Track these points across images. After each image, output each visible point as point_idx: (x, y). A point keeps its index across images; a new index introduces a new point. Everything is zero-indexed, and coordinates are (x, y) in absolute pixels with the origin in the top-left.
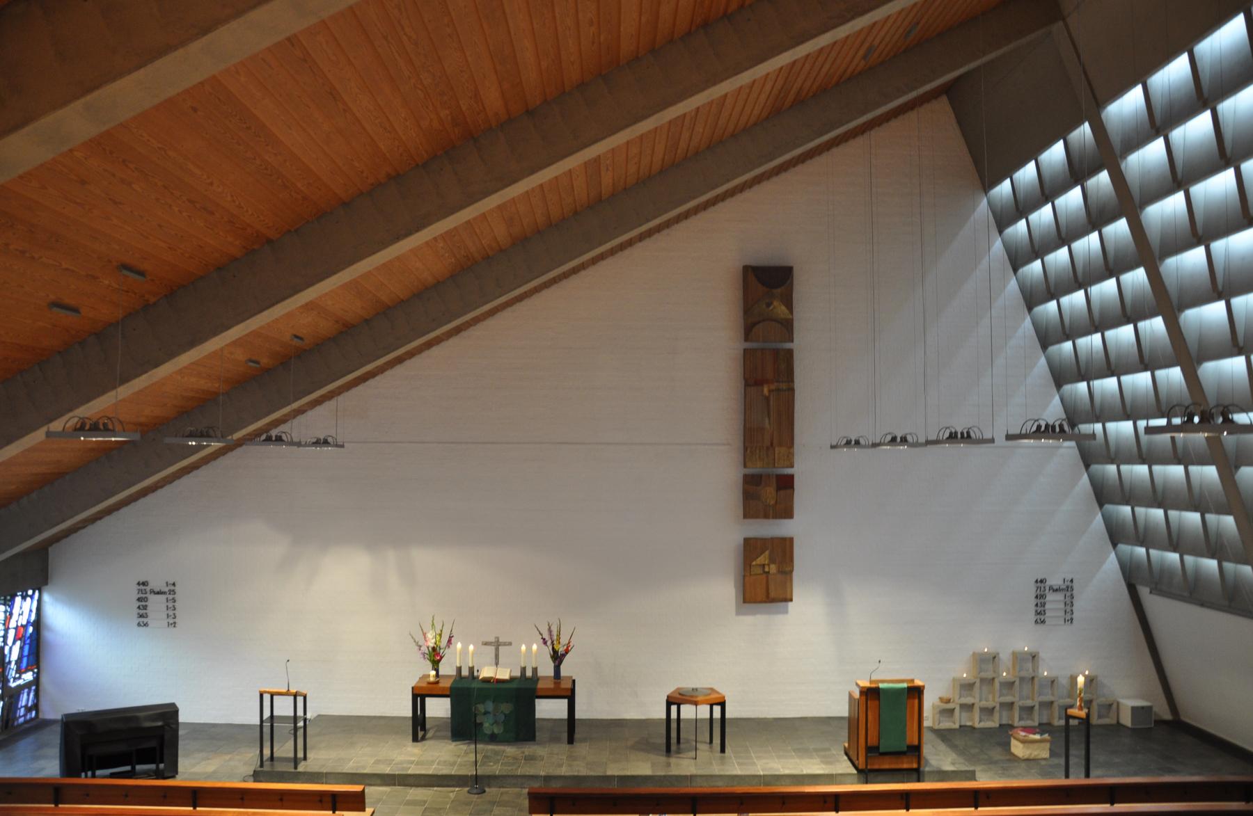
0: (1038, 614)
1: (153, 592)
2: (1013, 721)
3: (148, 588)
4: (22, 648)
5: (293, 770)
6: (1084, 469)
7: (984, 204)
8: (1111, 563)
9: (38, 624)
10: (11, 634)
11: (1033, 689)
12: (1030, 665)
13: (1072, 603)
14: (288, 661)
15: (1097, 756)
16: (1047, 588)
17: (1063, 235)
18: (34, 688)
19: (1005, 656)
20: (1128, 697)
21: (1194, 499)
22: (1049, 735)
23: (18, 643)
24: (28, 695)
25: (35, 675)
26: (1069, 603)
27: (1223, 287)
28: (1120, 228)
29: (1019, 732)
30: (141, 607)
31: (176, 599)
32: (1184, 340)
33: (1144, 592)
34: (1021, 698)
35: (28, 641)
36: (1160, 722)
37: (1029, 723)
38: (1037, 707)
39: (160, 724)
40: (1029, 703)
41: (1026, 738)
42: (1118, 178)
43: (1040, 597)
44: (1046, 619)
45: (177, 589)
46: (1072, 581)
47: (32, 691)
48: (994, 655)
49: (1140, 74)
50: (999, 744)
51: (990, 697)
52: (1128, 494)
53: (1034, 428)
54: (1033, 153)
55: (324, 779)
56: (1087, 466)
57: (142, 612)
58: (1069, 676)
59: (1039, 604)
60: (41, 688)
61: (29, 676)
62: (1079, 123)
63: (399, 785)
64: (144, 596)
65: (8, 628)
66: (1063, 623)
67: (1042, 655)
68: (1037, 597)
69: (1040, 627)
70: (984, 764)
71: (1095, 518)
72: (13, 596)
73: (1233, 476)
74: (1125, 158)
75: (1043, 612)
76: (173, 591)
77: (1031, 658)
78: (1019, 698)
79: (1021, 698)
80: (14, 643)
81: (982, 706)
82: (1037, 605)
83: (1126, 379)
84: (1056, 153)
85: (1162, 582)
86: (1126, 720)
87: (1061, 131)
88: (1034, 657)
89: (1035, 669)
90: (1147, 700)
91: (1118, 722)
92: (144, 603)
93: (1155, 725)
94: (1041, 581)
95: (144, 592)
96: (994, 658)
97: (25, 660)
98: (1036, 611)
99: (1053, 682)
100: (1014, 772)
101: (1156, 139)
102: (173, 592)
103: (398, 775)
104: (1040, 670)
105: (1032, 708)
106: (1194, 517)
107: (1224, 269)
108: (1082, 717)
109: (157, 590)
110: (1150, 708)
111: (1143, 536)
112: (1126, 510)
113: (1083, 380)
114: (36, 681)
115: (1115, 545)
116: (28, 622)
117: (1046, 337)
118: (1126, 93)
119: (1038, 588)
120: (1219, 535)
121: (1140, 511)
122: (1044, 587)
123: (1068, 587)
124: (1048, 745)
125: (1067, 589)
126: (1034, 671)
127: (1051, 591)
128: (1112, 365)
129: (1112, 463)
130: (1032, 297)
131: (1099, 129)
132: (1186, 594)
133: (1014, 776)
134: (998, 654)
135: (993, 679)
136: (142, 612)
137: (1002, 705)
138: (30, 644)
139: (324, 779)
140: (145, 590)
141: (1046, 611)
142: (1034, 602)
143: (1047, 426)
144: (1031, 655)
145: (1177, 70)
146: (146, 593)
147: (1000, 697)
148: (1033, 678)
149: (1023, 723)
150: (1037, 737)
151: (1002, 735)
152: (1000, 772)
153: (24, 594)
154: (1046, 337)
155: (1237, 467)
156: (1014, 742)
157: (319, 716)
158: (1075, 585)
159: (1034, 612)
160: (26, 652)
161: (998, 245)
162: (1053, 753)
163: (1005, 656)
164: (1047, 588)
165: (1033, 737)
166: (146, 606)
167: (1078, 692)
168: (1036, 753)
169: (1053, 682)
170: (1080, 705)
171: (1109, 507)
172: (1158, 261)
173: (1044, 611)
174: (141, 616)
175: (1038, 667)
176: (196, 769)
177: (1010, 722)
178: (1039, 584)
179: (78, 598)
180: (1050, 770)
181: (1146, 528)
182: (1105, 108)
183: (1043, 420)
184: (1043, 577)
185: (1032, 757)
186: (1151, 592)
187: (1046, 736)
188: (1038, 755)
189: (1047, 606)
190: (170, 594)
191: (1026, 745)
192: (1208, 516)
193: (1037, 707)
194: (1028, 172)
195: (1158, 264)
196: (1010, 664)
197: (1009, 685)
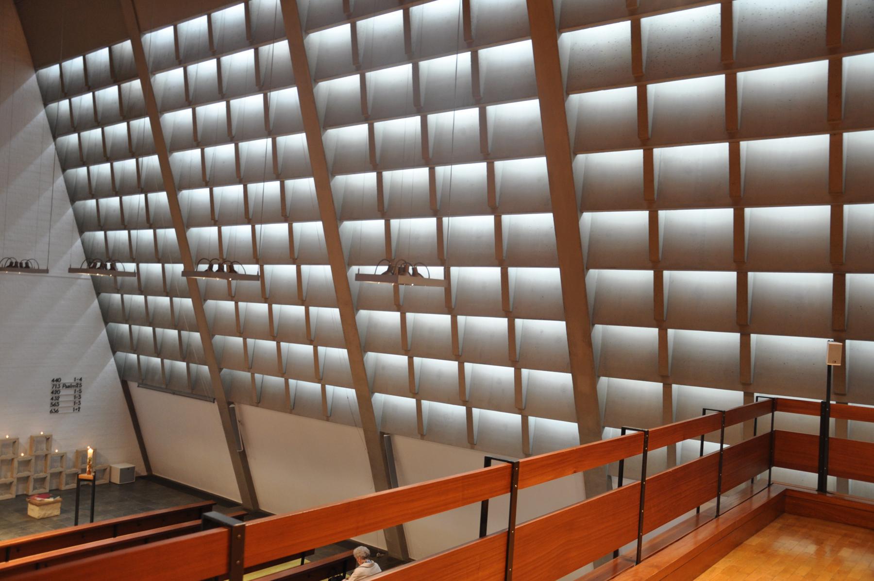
0: (53, 405)
2: (28, 491)
6: (95, 296)
7: (33, 78)
8: (111, 365)
11: (46, 464)
12: (44, 446)
13: (80, 396)
15: (98, 508)
16: (61, 386)
17: (99, 118)
19: (24, 441)
20: (119, 463)
21: (175, 321)
22: (60, 497)
26: (77, 399)
27: (210, 179)
28: (144, 124)
29: (36, 498)
32: (180, 210)
33: (133, 386)
34: (36, 472)
36: (140, 478)
37: (41, 491)
38: (48, 478)
40: (42, 475)
41: (42, 502)
42: (147, 87)
43: (55, 392)
44: (59, 410)
46: (81, 379)
48: (14, 441)
49: (174, 19)
50: (17, 511)
51: (9, 474)
52: (128, 316)
53: (8, 264)
54: (83, 50)
56: (98, 294)
58: (75, 451)
59: (54, 398)
62: (123, 39)
66: (73, 411)
67: (54, 437)
68: (52, 393)
69: (55, 415)
70: (4, 528)
71: (101, 333)
73: (202, 305)
74: (154, 74)
75: (57, 404)
77: (45, 439)
78: (32, 473)
79: (36, 472)
81: (35, 477)
82: (52, 399)
83: (111, 234)
84: (101, 56)
85: (147, 379)
86: (116, 479)
87: (109, 42)
88: (48, 439)
89: (16, 453)
90: (131, 463)
91: (110, 482)
93: (136, 480)
94: (57, 380)
96: (14, 442)
98: (51, 404)
99: (62, 457)
100: (31, 530)
101: (179, 68)
104: (52, 450)
105: (44, 479)
106: (174, 333)
107: (211, 167)
108: (90, 479)
110: (133, 468)
111: (136, 346)
112: (125, 327)
113: (101, 230)
115: (114, 352)
117: (75, 193)
118: (161, 29)
119: (54, 385)
120: (189, 345)
121: (135, 328)
122: (59, 385)
123: (77, 384)
124: (59, 505)
125: (77, 386)
126: (47, 450)
127: (64, 388)
128: (124, 222)
129: (118, 293)
130: (66, 161)
131: (138, 47)
132: (164, 386)
133: (32, 533)
134: (18, 439)
135: (13, 459)
137: (19, 479)
141: (59, 403)
142: (50, 396)
143: (16, 263)
144: (46, 437)
145: (196, 25)
147: (18, 472)
148: (46, 455)
149: (36, 492)
150: (51, 500)
151: (21, 502)
152: (20, 532)
154: (75, 193)
155: (205, 300)
156: (30, 507)
158: (83, 383)
159: (50, 403)
161: (41, 115)
162: (63, 511)
163: (24, 441)
164: (61, 386)
165: (47, 500)
167: (88, 461)
168: (49, 512)
169: (62, 457)
170: (89, 471)
171: (112, 325)
172: (168, 153)
173: (58, 403)
175: (51, 447)
177: (25, 493)
178: (55, 383)
180: (62, 523)
181: (139, 340)
182: (145, 34)
183: (14, 258)
184: (58, 377)
185: (47, 515)
186: (138, 386)
187: (58, 498)
188: (45, 513)
189: (60, 399)
191: (42, 507)
192: (183, 333)
193: (48, 478)
194: (75, 64)
195: (168, 155)
196: (27, 446)
197: (26, 463)
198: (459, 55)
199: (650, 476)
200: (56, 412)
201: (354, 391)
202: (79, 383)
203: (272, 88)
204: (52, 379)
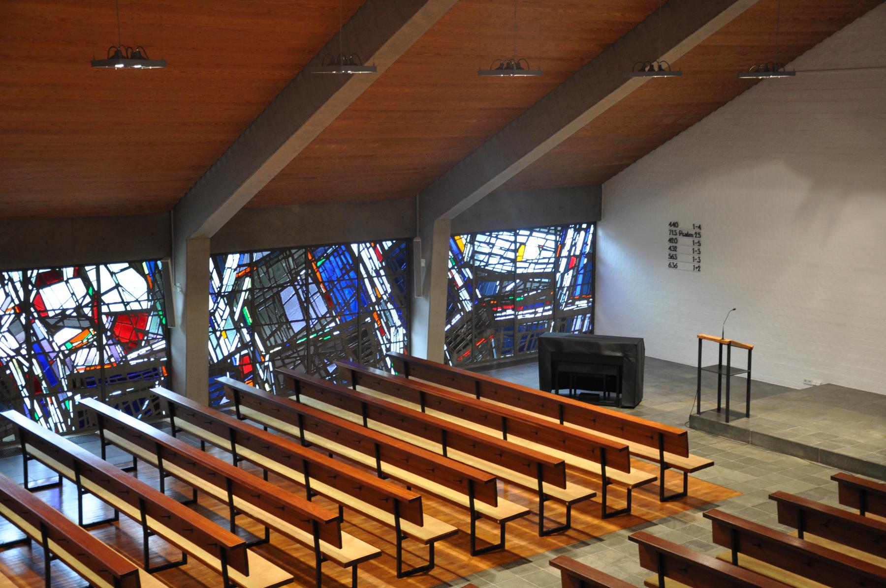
1: (681, 233)
3: (678, 230)
4: (575, 278)
5: (724, 423)
9: (593, 256)
10: (563, 263)
14: (734, 309)
18: (588, 315)
23: (571, 272)
24: (583, 321)
25: (590, 304)
30: (672, 248)
31: (701, 242)
35: (582, 271)
39: (619, 354)
45: (702, 232)
47: (587, 318)
55: (750, 438)
57: (673, 253)
60: (596, 317)
61: (583, 304)
63: (821, 462)
64: (674, 237)
65: (560, 257)
72: (565, 229)
76: (699, 234)
80: (567, 270)
92: (674, 245)
95: (674, 233)
97: (579, 288)
102: (698, 235)
103: (821, 450)
109: (685, 232)
114: (592, 309)
116: (582, 253)
127: (681, 235)
136: (673, 253)
138: (584, 274)
139: (750, 438)
140: (675, 231)
146: (676, 235)
153: (578, 226)
157: (829, 385)
160: (580, 281)
164: (678, 232)
166: (676, 247)
174: (672, 257)
176: (657, 407)
179: (621, 237)
190: (696, 237)
198: (91, 281)
199: (658, 545)
200: (674, 266)
201: (230, 257)
202: (698, 232)
203: (785, 65)
204: (669, 223)
